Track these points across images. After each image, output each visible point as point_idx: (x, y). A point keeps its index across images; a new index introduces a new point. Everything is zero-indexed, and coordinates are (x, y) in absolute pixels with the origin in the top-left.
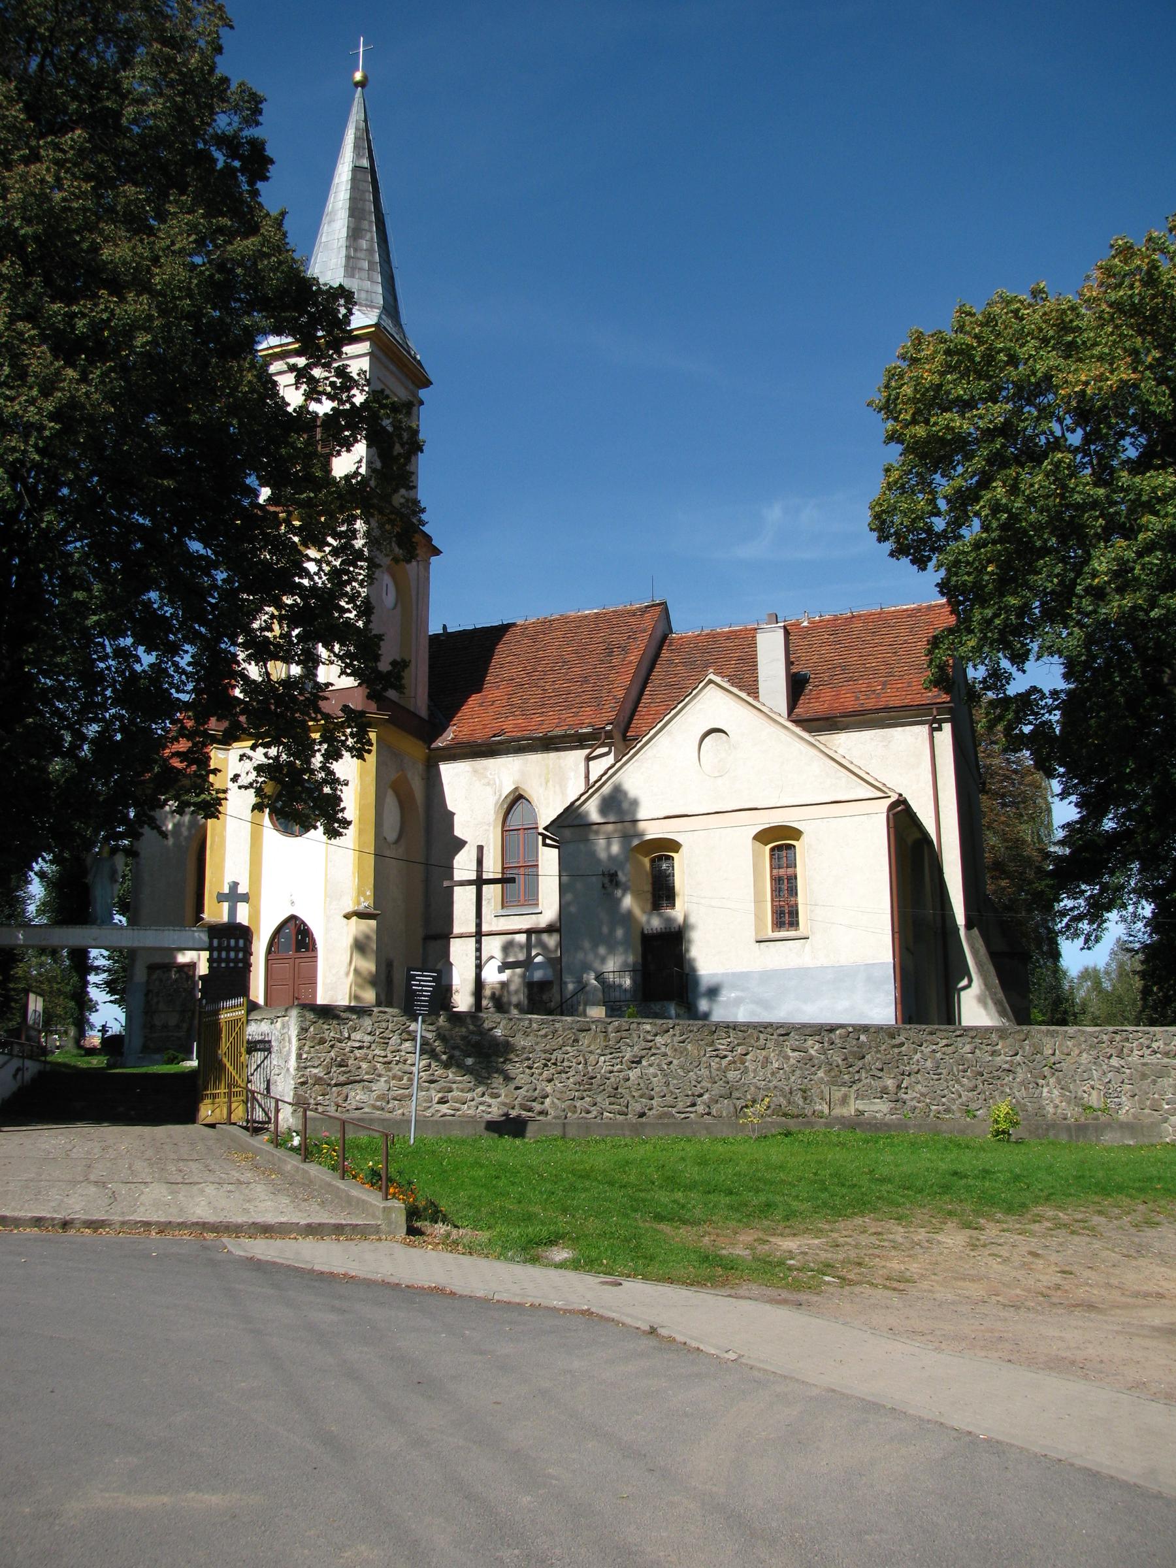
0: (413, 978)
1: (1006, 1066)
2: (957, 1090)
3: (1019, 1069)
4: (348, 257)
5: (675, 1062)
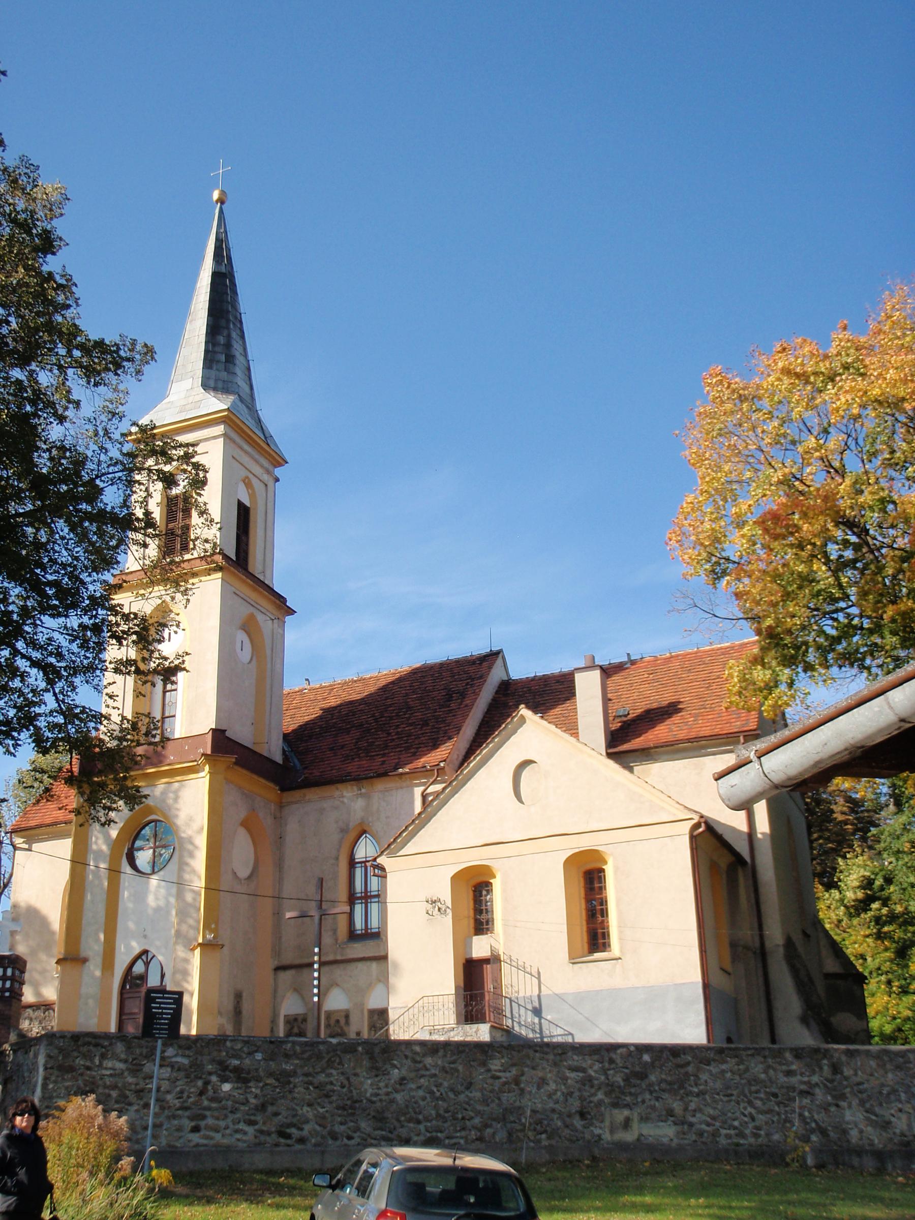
0: (153, 1000)
1: (803, 1087)
2: (750, 1114)
3: (817, 1091)
5: (446, 1084)
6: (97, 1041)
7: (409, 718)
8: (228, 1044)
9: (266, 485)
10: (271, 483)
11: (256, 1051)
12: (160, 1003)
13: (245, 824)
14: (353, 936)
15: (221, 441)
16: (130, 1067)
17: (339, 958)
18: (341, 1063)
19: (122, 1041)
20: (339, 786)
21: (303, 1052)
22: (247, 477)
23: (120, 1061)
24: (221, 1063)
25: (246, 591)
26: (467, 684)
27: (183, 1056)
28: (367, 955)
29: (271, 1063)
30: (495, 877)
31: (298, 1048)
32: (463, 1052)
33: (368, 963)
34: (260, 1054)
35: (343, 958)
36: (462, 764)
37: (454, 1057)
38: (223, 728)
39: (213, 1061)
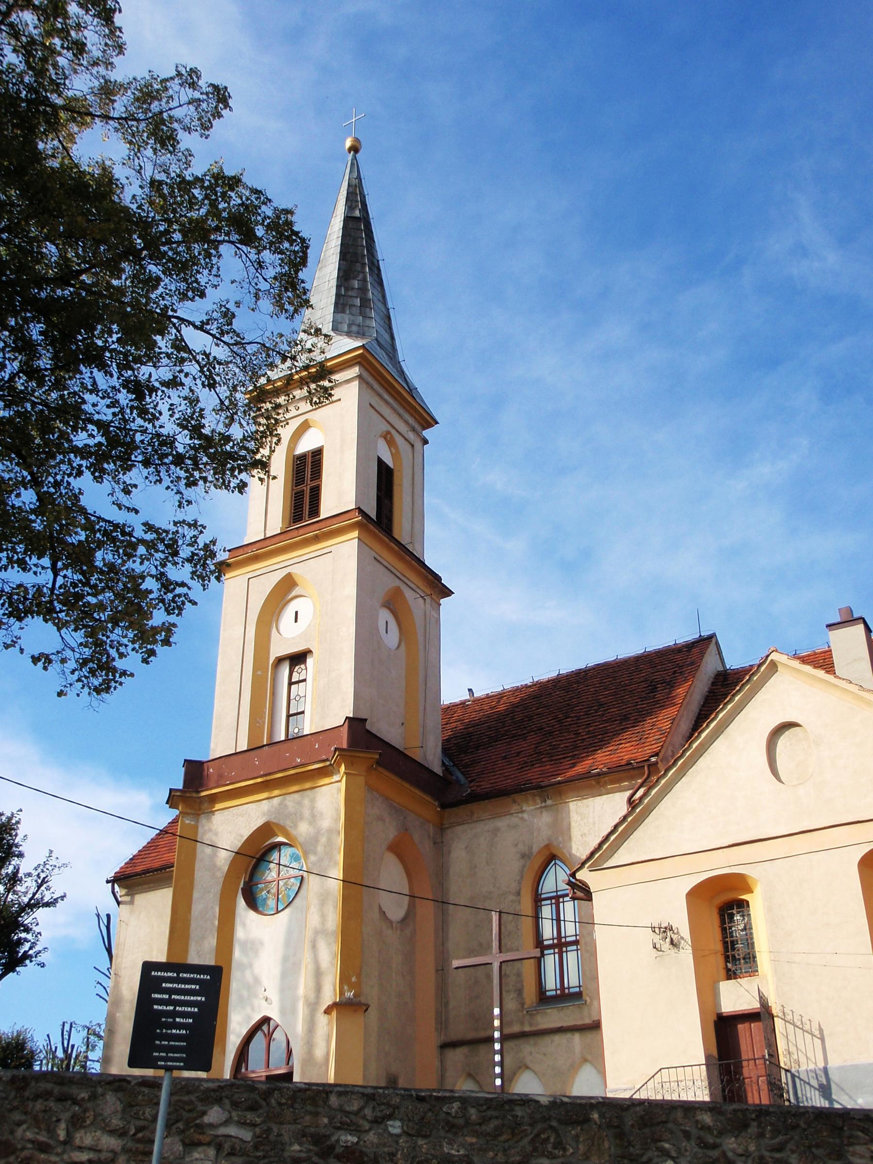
4: (338, 295)
6: (65, 1089)
7: (603, 715)
8: (334, 1100)
9: (413, 446)
10: (418, 444)
11: (391, 1117)
12: (170, 991)
13: (395, 848)
14: (544, 998)
15: (356, 383)
16: (130, 1145)
17: (527, 1028)
18: (559, 1145)
19: (116, 1091)
20: (517, 797)
21: (484, 1121)
22: (388, 433)
23: (112, 1132)
24: (318, 1139)
25: (388, 558)
26: (675, 672)
27: (242, 1124)
28: (565, 1024)
29: (420, 1142)
30: (750, 891)
31: (473, 1112)
32: (795, 1127)
33: (569, 1035)
34: (398, 1123)
35: (534, 1029)
36: (691, 735)
37: (780, 1138)
38: (364, 717)
39: (301, 1136)
